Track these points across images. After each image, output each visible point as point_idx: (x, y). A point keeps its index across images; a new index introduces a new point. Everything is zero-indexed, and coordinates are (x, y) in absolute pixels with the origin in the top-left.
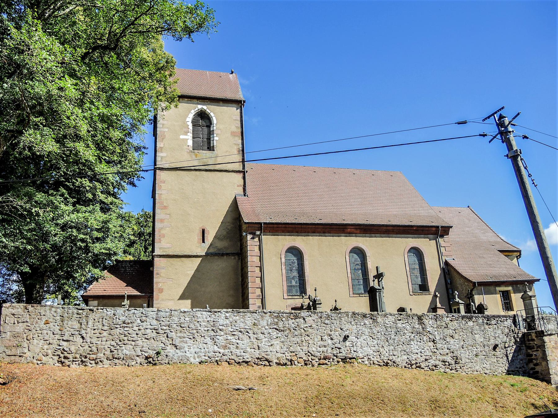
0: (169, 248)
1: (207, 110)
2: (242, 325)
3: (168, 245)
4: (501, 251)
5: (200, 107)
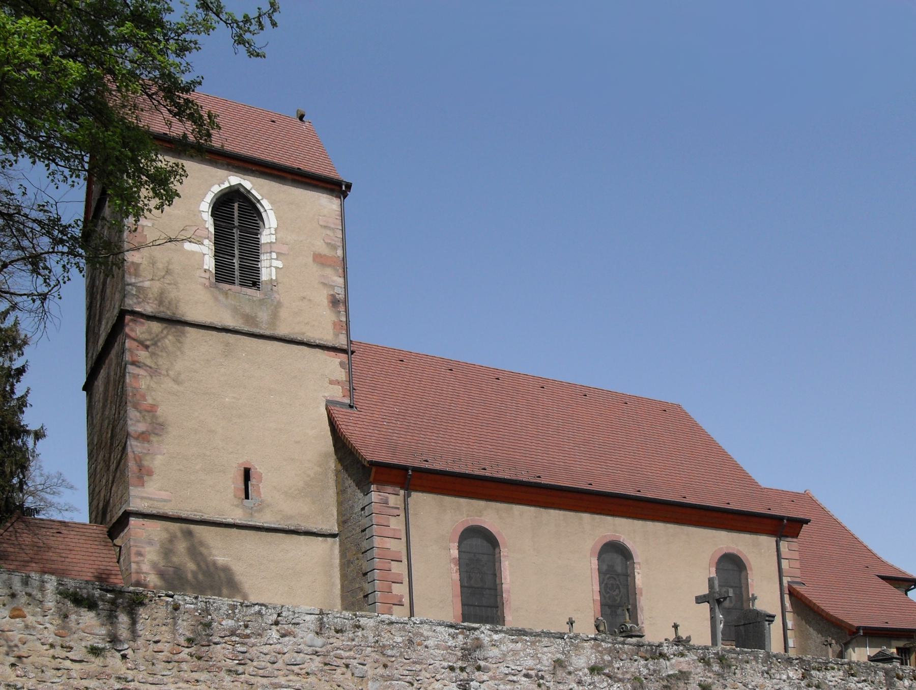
0: (165, 501)
1: (253, 192)
2: (530, 662)
3: (164, 495)
4: (879, 576)
5: (234, 180)
